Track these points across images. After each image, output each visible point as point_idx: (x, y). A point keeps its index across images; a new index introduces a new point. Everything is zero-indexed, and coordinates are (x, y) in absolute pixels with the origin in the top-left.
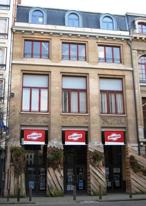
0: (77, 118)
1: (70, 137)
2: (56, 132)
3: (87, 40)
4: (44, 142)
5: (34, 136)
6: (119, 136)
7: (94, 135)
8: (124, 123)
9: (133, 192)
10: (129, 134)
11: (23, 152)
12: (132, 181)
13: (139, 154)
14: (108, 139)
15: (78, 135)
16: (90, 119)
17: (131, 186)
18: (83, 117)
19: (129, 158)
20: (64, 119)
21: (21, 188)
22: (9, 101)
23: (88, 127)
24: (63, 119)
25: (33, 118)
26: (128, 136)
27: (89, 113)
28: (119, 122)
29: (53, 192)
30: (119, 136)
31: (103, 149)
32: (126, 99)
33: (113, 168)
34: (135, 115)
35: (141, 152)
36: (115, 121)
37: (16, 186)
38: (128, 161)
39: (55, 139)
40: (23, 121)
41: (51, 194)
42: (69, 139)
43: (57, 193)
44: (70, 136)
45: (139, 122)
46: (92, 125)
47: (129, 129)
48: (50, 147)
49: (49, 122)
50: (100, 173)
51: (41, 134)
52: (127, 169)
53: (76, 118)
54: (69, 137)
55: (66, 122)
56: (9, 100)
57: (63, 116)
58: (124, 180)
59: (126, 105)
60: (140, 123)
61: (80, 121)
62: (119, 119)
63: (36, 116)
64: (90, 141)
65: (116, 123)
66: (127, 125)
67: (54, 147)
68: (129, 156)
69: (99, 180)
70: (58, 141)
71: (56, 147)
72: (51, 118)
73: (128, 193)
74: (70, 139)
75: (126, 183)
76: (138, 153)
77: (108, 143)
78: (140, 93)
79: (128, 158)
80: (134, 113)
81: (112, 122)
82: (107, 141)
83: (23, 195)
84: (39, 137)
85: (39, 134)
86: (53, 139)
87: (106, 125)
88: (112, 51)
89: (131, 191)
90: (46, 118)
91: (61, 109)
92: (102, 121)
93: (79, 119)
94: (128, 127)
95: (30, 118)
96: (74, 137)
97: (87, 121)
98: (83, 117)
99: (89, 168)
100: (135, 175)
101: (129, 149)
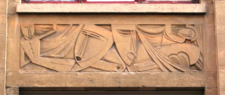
0: (126, 32)
3: (76, 57)
11: (136, 32)
16: (214, 37)
18: (168, 23)
20: (37, 40)
24: (25, 43)
53: (118, 37)
55: (46, 62)
57: (29, 22)
61: (142, 54)
88: (95, 32)
93: (139, 41)
98: (168, 29)
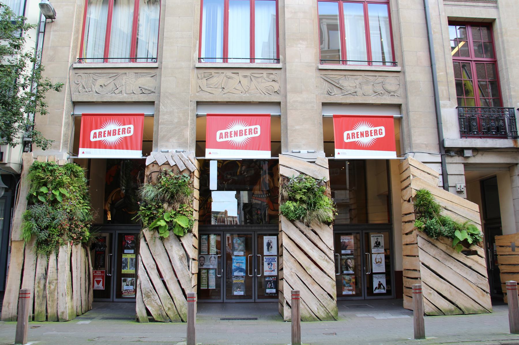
0: (245, 77)
1: (221, 134)
2: (176, 120)
4: (395, 152)
5: (236, 134)
6: (382, 131)
7: (297, 127)
8: (394, 92)
9: (428, 308)
10: (412, 124)
12: (424, 274)
13: (445, 187)
14: (92, 139)
15: (373, 129)
17: (419, 290)
19: (413, 199)
21: (54, 289)
22: (41, 35)
23: (279, 104)
24: (200, 81)
25: (111, 80)
26: (409, 131)
27: (285, 63)
28: (379, 89)
29: (153, 306)
30: (382, 131)
31: (328, 171)
32: (399, 23)
33: (261, 237)
34: (428, 69)
35: (451, 180)
36: (365, 87)
37: (39, 283)
38: (409, 207)
39: (174, 140)
40: (81, 88)
41: (149, 313)
42: (346, 140)
43: (169, 309)
44: (350, 132)
45: (442, 89)
46: (291, 98)
47: (411, 108)
48: (155, 163)
49: (157, 91)
50: (316, 246)
51: (258, 127)
52: (407, 234)
54: (347, 136)
56: (42, 30)
58: (398, 268)
59: (401, 38)
60: (445, 93)
62: (380, 80)
63: (117, 75)
64: (286, 146)
65: (371, 92)
66: (406, 97)
67: (167, 164)
68: (414, 193)
69: (313, 270)
70: (180, 145)
71: (172, 163)
72: (163, 79)
73: (410, 311)
74: (221, 140)
75: (404, 279)
76: (441, 185)
77: (345, 154)
78: (441, 6)
79: (409, 201)
80: (425, 62)
81: (358, 90)
82: (341, 148)
83: (59, 314)
84: (254, 135)
85: (253, 127)
86: (168, 141)
87: (338, 98)
89: (419, 303)
90: (149, 78)
91: (195, 51)
92: (326, 85)
94: (407, 104)
95: (101, 81)
96: (362, 134)
97: (276, 86)
98: (265, 75)
99: (282, 231)
100: (433, 251)
101: (412, 170)
